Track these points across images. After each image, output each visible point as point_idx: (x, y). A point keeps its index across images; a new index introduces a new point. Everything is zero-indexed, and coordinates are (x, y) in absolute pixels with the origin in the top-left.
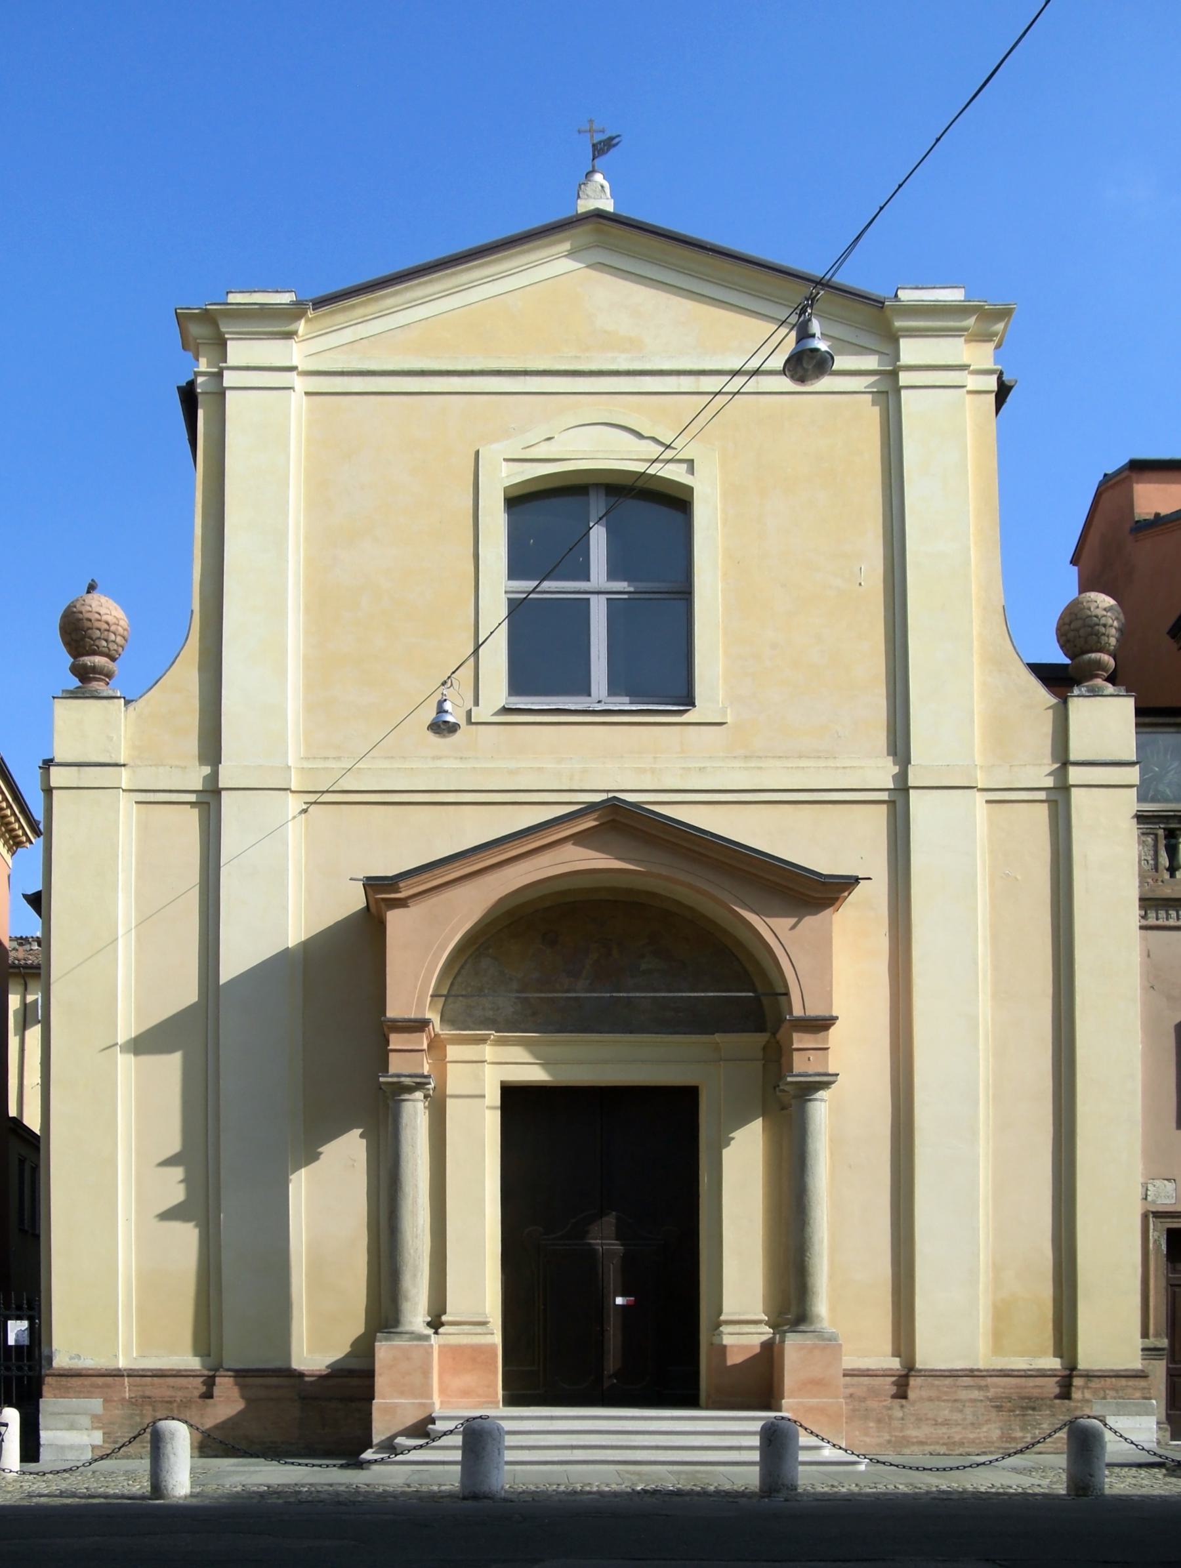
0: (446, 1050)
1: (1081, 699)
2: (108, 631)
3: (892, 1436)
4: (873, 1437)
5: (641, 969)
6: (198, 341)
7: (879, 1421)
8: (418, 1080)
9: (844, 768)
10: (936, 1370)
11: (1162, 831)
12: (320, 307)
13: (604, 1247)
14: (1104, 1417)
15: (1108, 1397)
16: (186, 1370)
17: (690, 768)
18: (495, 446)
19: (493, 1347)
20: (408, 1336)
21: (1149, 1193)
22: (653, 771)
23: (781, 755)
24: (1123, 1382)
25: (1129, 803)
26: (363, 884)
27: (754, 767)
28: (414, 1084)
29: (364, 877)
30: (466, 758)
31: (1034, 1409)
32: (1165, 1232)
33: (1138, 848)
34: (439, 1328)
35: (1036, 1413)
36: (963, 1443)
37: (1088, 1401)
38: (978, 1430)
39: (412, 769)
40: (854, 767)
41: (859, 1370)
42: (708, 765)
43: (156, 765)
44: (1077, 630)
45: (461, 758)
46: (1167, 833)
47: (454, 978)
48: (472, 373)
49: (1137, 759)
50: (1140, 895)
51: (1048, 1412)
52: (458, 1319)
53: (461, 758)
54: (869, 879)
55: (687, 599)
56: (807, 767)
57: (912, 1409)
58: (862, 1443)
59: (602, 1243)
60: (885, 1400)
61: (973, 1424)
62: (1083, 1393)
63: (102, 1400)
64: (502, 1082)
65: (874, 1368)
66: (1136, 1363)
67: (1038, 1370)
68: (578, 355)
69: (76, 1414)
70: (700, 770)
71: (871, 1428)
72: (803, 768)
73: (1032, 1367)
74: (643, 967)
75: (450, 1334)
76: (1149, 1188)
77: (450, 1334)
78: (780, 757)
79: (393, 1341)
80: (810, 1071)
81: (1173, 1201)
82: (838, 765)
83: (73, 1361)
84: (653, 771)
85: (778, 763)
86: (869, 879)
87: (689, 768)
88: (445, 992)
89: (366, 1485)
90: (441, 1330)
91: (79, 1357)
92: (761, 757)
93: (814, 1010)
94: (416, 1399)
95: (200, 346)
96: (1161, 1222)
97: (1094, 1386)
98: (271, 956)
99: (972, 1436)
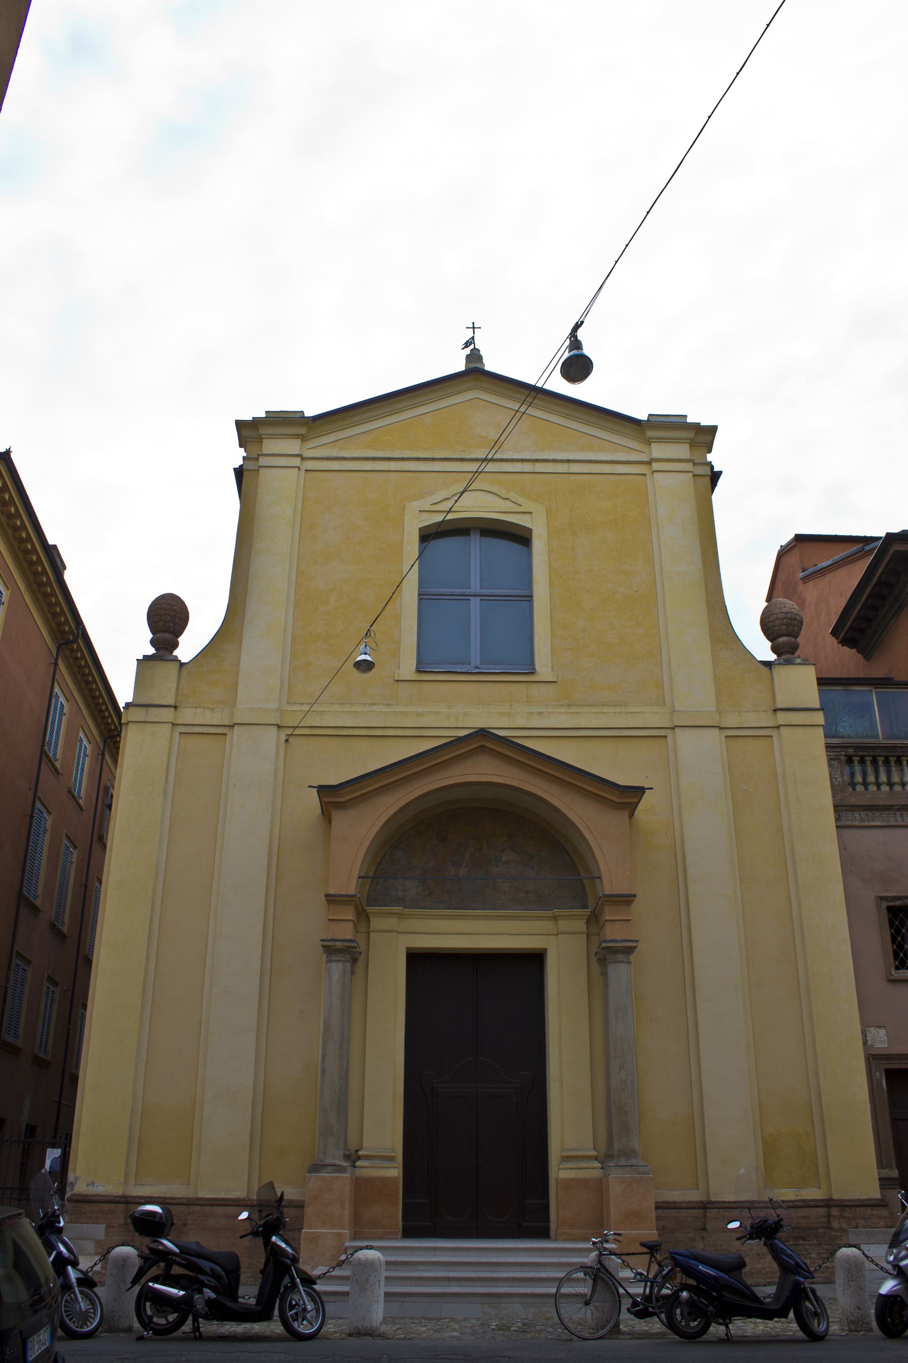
0: (821, 703)
1: (780, 666)
2: (176, 616)
6: (247, 440)
8: (347, 944)
9: (632, 713)
10: (726, 1202)
11: (843, 757)
12: (318, 420)
14: (859, 1246)
15: (859, 1225)
16: (170, 1198)
17: (532, 713)
18: (415, 503)
19: (394, 1180)
20: (331, 1168)
21: (868, 1038)
22: (509, 714)
23: (591, 704)
24: (869, 1211)
25: (817, 740)
26: (317, 791)
27: (573, 712)
29: (318, 785)
30: (390, 705)
31: (804, 1239)
32: (884, 1073)
33: (829, 770)
35: (805, 1243)
36: (752, 1273)
37: (844, 1230)
38: (763, 1261)
39: (356, 712)
40: (639, 712)
41: (668, 1202)
42: (544, 710)
43: (195, 708)
44: (773, 621)
45: (387, 705)
46: (846, 758)
47: (378, 866)
48: (403, 459)
49: (821, 706)
50: (834, 803)
51: (815, 1242)
52: (371, 1153)
53: (387, 705)
54: (652, 788)
55: (530, 601)
56: (608, 712)
57: (711, 1240)
60: (690, 1232)
61: (758, 1254)
62: (840, 1223)
63: (105, 1225)
64: (407, 949)
66: (873, 1192)
67: (803, 1201)
68: (464, 450)
69: (85, 1239)
72: (606, 713)
73: (799, 1198)
74: (504, 859)
76: (868, 1035)
79: (320, 1172)
80: (618, 938)
81: (886, 1046)
82: (628, 711)
83: (89, 1187)
84: (509, 714)
85: (587, 709)
86: (652, 788)
87: (532, 713)
88: (371, 875)
91: (93, 1184)
93: (621, 888)
95: (248, 443)
96: (879, 1064)
97: (847, 1216)
99: (758, 1266)
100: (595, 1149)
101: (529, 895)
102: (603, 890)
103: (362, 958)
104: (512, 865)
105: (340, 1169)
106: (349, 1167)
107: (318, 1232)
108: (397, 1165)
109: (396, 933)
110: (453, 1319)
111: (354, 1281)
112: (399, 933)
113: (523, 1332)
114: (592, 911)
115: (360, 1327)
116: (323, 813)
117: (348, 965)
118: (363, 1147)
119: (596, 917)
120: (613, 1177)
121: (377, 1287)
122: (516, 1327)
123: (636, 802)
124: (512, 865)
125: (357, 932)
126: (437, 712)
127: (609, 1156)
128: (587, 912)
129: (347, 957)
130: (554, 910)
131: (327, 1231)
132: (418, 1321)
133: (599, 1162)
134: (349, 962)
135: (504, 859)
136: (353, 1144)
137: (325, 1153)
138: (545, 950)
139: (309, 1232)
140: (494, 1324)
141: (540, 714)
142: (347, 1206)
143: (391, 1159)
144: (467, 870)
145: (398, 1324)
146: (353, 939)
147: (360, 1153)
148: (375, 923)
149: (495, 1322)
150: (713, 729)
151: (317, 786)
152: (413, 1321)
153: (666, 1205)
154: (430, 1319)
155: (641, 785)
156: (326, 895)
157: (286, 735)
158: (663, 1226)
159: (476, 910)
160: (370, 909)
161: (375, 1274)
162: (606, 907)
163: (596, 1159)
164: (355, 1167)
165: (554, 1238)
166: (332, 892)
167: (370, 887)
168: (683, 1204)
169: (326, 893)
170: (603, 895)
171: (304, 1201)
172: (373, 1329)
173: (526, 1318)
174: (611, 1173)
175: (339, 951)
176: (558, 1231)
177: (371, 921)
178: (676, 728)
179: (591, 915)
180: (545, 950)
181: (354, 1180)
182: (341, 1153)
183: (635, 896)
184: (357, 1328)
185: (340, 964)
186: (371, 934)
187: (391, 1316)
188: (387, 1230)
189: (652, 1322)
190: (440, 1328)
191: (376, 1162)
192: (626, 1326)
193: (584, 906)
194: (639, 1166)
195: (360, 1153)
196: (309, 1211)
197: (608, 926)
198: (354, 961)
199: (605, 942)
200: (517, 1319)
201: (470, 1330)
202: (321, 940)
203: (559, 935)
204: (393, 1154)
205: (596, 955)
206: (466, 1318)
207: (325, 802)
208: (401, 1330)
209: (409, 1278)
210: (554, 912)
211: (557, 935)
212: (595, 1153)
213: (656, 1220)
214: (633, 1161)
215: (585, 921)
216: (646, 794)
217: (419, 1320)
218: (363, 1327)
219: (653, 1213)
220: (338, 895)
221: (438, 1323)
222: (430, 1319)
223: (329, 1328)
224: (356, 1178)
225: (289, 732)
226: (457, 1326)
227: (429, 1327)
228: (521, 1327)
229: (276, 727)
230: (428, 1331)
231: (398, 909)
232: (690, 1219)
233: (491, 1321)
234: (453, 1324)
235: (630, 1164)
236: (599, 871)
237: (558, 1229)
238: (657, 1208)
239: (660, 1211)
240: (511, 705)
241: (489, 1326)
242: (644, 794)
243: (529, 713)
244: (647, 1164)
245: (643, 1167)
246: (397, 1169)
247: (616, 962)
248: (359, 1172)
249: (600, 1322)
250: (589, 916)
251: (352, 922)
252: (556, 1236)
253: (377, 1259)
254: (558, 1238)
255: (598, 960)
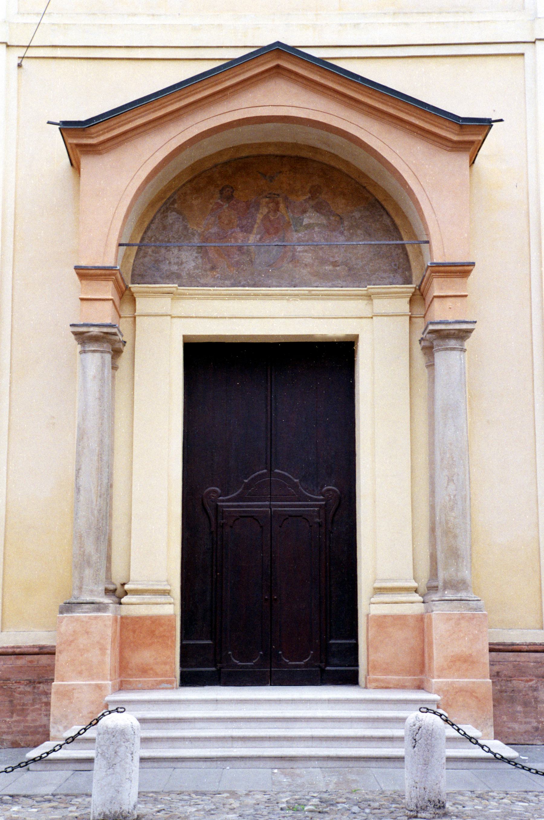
3: (539, 722)
4: (521, 723)
5: (304, 224)
7: (526, 704)
8: (105, 330)
9: (479, 22)
13: (273, 509)
19: (170, 618)
20: (88, 606)
26: (60, 129)
28: (102, 334)
29: (61, 122)
34: (123, 597)
39: (111, 25)
40: (488, 21)
41: (504, 644)
45: (153, 15)
47: (145, 232)
52: (140, 587)
54: (501, 120)
56: (446, 22)
58: (510, 730)
59: (270, 504)
60: (531, 680)
64: (184, 336)
65: (518, 642)
70: (355, 26)
71: (517, 712)
74: (306, 221)
75: (132, 604)
77: (132, 604)
78: (423, 13)
80: (450, 319)
86: (501, 120)
87: (345, 25)
89: (10, 796)
90: (124, 600)
92: (406, 13)
94: (93, 679)
98: (198, 334)
100: (415, 579)
101: (338, 268)
102: (432, 258)
103: (126, 350)
104: (316, 229)
105: (100, 607)
106: (111, 605)
107: (73, 684)
108: (172, 600)
109: (169, 318)
110: (233, 794)
111: (99, 754)
112: (175, 317)
113: (320, 812)
114: (417, 288)
115: (107, 813)
116: (72, 164)
117: (108, 357)
118: (131, 578)
119: (422, 295)
120: (437, 614)
121: (129, 760)
122: (312, 805)
123: (480, 140)
124: (316, 229)
125: (120, 317)
126: (219, 25)
127: (432, 589)
128: (410, 288)
129: (106, 346)
130: (368, 287)
131: (84, 683)
132: (187, 798)
133: (420, 595)
134: (109, 352)
135: (306, 221)
136: (118, 577)
137: (80, 588)
138: (357, 336)
139: (61, 685)
140: (284, 799)
141: (356, 25)
142: (109, 652)
143: (166, 593)
144: (258, 237)
145: (161, 803)
146: (113, 324)
147: (126, 587)
148: (142, 304)
149: (286, 797)
150: (526, 44)
151: (58, 122)
152: (182, 797)
153: (501, 647)
154: (204, 794)
155: (487, 117)
156: (77, 268)
157: (19, 57)
158: (498, 673)
159: (270, 287)
160: (135, 288)
161: (126, 744)
162: (435, 280)
163: (416, 591)
164: (120, 604)
165: (363, 686)
166: (83, 263)
167: (134, 261)
168: (524, 647)
169: (75, 265)
170: (431, 264)
171: (54, 647)
172: (124, 814)
173: (325, 790)
174: (434, 608)
175: (95, 339)
176: (368, 677)
177: (137, 303)
178: (537, 42)
179: (414, 292)
180: (357, 336)
181: (119, 620)
182: (101, 588)
183: (473, 264)
184: (103, 814)
185: (97, 355)
186: (137, 318)
187: (154, 790)
188: (160, 679)
189: (487, 797)
190: (214, 807)
191: (147, 598)
192: (454, 804)
193: (408, 281)
194: (469, 601)
195: (126, 587)
196: (61, 660)
197: (437, 304)
198: (116, 353)
199: (432, 323)
200: (314, 793)
201: (252, 811)
202: (71, 325)
203: (374, 318)
204: (168, 588)
205: (420, 343)
206: (250, 792)
207: (70, 144)
208: (163, 812)
209: (183, 739)
210: (369, 288)
211: (372, 318)
212: (415, 585)
213: (490, 664)
214: (463, 595)
215: (408, 299)
216: (493, 127)
217: (189, 795)
218: (111, 813)
219: (486, 657)
220: (92, 267)
221: (213, 800)
222: (204, 794)
223: (71, 812)
224: (122, 618)
225: (21, 52)
226: (236, 804)
227: (200, 807)
228: (318, 805)
229: (5, 46)
230: (197, 813)
231: (172, 287)
232: (532, 664)
233: (281, 795)
234: (231, 801)
235: (459, 598)
236: (428, 235)
237: (368, 675)
238: (491, 650)
239: (494, 654)
240: (317, 14)
241: (277, 803)
242: (490, 128)
243: (341, 25)
244: (479, 599)
245: (475, 602)
246: (172, 605)
247: (447, 349)
248: (125, 610)
249: (420, 802)
250: (414, 294)
251: (111, 302)
252: (366, 682)
253: (130, 726)
254: (368, 686)
255: (423, 348)
